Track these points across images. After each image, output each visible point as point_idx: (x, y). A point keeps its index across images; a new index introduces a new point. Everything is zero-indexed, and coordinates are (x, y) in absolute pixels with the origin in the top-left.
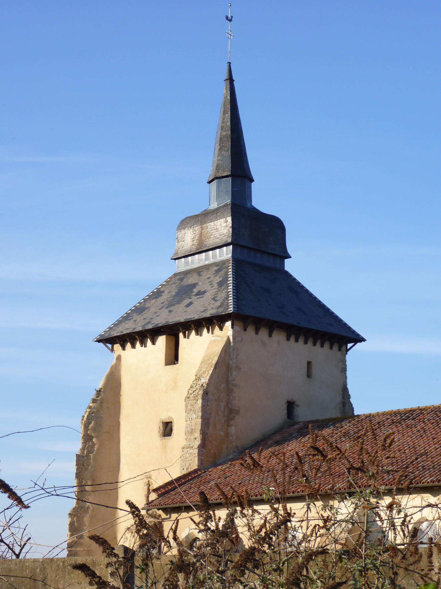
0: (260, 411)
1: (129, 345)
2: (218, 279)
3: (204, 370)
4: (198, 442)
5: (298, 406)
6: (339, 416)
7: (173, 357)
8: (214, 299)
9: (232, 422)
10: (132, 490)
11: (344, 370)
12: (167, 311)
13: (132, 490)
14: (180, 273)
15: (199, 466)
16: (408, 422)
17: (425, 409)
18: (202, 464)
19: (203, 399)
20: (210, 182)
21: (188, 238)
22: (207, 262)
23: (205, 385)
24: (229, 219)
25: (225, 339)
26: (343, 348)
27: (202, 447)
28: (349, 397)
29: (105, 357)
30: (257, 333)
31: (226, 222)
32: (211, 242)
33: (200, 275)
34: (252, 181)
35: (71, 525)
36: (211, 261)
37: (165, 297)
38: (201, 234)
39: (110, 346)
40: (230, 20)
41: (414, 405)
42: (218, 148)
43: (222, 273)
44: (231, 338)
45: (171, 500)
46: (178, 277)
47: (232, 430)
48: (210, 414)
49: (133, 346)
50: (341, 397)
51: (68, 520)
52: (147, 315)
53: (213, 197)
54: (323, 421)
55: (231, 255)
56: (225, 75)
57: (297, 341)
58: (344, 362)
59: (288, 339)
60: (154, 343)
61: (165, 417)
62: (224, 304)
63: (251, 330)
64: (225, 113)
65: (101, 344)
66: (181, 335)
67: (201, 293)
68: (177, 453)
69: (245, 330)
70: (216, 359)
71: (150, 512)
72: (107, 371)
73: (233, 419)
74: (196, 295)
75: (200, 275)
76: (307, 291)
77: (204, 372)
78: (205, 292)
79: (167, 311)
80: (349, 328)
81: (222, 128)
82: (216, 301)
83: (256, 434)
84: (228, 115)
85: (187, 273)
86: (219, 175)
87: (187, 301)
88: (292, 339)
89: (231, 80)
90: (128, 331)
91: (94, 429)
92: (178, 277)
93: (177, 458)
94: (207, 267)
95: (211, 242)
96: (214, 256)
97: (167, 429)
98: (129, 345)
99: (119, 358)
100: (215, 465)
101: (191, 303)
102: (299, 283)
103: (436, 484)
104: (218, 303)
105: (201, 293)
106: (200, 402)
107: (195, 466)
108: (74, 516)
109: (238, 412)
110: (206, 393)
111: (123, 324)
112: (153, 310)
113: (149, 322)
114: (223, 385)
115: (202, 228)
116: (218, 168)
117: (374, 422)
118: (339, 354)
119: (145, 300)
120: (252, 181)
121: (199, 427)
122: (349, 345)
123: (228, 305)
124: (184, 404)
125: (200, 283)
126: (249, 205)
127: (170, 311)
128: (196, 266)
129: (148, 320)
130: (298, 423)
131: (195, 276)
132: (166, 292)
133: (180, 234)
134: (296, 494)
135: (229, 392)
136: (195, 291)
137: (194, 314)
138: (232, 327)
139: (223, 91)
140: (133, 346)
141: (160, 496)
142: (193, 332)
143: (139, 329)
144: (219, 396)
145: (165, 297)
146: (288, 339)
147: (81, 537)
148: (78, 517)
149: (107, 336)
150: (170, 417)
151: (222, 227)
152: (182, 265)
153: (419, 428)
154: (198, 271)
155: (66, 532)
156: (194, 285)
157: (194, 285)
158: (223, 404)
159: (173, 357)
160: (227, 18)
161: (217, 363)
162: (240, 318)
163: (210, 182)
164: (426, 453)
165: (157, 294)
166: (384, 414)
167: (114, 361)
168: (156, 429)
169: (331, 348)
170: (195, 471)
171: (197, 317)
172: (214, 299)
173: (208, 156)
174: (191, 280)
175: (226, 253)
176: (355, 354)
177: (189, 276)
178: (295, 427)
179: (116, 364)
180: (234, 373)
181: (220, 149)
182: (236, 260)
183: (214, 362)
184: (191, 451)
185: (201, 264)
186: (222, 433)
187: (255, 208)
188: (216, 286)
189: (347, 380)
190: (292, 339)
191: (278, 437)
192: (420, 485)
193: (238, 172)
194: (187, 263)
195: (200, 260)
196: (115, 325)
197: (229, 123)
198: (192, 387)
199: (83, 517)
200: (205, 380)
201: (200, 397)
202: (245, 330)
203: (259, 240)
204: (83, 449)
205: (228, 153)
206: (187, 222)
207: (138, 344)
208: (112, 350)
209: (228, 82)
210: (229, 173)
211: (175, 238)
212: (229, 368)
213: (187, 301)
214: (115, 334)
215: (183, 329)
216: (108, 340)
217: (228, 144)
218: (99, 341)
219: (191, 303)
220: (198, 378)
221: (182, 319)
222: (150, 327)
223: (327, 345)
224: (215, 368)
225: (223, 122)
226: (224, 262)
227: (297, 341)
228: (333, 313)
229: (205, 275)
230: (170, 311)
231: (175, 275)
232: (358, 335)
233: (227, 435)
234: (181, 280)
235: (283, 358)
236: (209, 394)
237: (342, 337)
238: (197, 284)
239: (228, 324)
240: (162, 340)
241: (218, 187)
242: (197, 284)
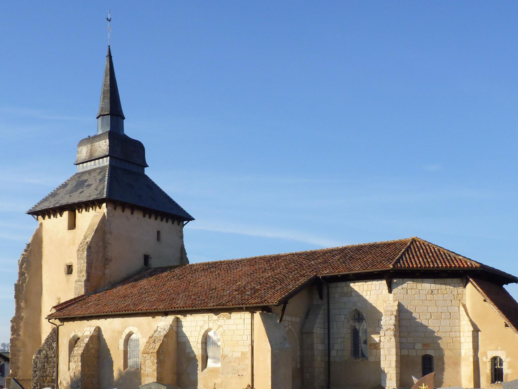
0: (125, 260)
1: (47, 217)
2: (100, 177)
3: (89, 233)
4: (85, 278)
5: (151, 258)
6: (178, 264)
7: (72, 225)
8: (96, 189)
9: (107, 266)
10: (47, 306)
11: (182, 237)
12: (68, 196)
13: (47, 306)
14: (79, 173)
15: (85, 293)
16: (212, 270)
17: (223, 262)
18: (87, 292)
19: (88, 251)
20: (98, 118)
21: (84, 152)
22: (95, 167)
23: (89, 242)
24: (107, 141)
25: (102, 214)
26: (181, 224)
27: (87, 281)
28: (186, 254)
29: (32, 224)
30: (123, 212)
31: (106, 142)
32: (97, 155)
33: (90, 175)
34: (124, 118)
35: (12, 327)
36: (97, 166)
37: (69, 187)
38: (91, 150)
39: (36, 217)
40: (110, 21)
41: (218, 260)
42: (102, 97)
43: (102, 174)
44: (106, 214)
45: (66, 313)
46: (78, 176)
47: (107, 271)
48: (93, 260)
49: (49, 217)
50: (180, 254)
51: (10, 324)
52: (57, 198)
53: (100, 127)
54: (164, 268)
55: (108, 163)
56: (107, 53)
57: (150, 218)
58: (181, 232)
59: (144, 216)
60: (61, 216)
61: (68, 262)
62: (101, 193)
63: (119, 210)
64: (106, 76)
65: (30, 215)
66: (77, 211)
67: (89, 186)
68: (73, 285)
69: (115, 209)
70: (96, 226)
71: (50, 321)
72: (34, 232)
73: (108, 264)
74: (86, 187)
75: (90, 175)
76: (159, 187)
77: (89, 234)
78: (91, 185)
79: (68, 196)
80: (185, 211)
81: (105, 85)
82: (97, 190)
83: (123, 274)
84: (108, 77)
85: (83, 173)
86: (103, 114)
87: (81, 190)
88: (147, 216)
89: (110, 56)
90: (45, 208)
91: (26, 268)
92: (78, 176)
93: (71, 288)
94: (94, 170)
95: (97, 154)
96: (99, 164)
97: (69, 269)
98: (47, 217)
99: (41, 225)
100: (95, 293)
101: (83, 191)
102: (153, 183)
103: (216, 307)
104: (98, 192)
105: (89, 186)
106: (85, 253)
107: (82, 293)
108: (14, 322)
109: (111, 260)
110: (89, 248)
111: (43, 204)
112: (61, 195)
113: (58, 203)
114: (101, 243)
115: (92, 146)
116: (102, 109)
117: (193, 269)
118: (178, 227)
119: (58, 189)
120: (124, 118)
121: (85, 269)
122: (185, 222)
123: (103, 193)
124: (76, 253)
125: (89, 180)
126: (122, 133)
127: (70, 196)
128: (89, 169)
129: (57, 201)
130: (150, 269)
131: (87, 175)
132: (70, 184)
133: (80, 149)
134: (135, 312)
135: (105, 247)
136: (86, 184)
137: (83, 198)
138: (107, 207)
139: (106, 63)
140: (49, 217)
141: (57, 311)
142: (84, 210)
143: (52, 206)
144: (98, 250)
145: (69, 187)
146: (144, 216)
147: (19, 335)
148: (16, 323)
149: (33, 210)
150: (71, 263)
151: (103, 146)
152: (81, 168)
153: (216, 273)
154: (89, 172)
155: (10, 332)
156: (86, 181)
157: (86, 181)
158: (101, 255)
159: (72, 225)
160: (107, 19)
161: (96, 229)
162: (111, 200)
163: (98, 118)
164: (215, 289)
165: (64, 186)
166: (200, 264)
167: (38, 227)
168: (63, 269)
169: (173, 223)
170: (82, 296)
171: (85, 200)
172: (96, 189)
173: (97, 102)
174: (84, 178)
175: (106, 162)
176: (188, 228)
177: (84, 175)
178: (149, 271)
179: (39, 228)
180: (108, 236)
181: (103, 98)
182: (112, 166)
183: (95, 228)
184: (80, 283)
185: (92, 168)
186: (101, 273)
187: (125, 135)
188: (98, 181)
189: (184, 243)
190: (147, 216)
191: (137, 277)
192: (206, 308)
193: (115, 112)
194: (83, 167)
195: (91, 166)
196: (39, 204)
197: (109, 82)
198: (81, 243)
199: (19, 323)
200: (89, 239)
201: (85, 250)
202: (115, 209)
203: (127, 156)
204: (19, 280)
205: (108, 101)
206: (83, 142)
207: (52, 216)
208: (37, 219)
209: (108, 57)
210: (109, 113)
211: (82, 153)
212: (104, 232)
213: (81, 190)
214: (38, 209)
215: (78, 207)
216: (37, 213)
217: (108, 95)
218: (29, 213)
219: (83, 191)
220: (85, 238)
221: (76, 201)
222: (58, 205)
223: (170, 222)
224: (96, 232)
225: (105, 82)
226: (104, 167)
227: (150, 218)
228: (174, 202)
229: (93, 175)
230: (70, 196)
231: (76, 174)
232: (190, 216)
233: (104, 274)
234: (79, 177)
235: (142, 229)
236: (92, 248)
237: (181, 217)
238: (87, 180)
239: (104, 205)
240: (66, 214)
241: (102, 121)
242: (87, 180)
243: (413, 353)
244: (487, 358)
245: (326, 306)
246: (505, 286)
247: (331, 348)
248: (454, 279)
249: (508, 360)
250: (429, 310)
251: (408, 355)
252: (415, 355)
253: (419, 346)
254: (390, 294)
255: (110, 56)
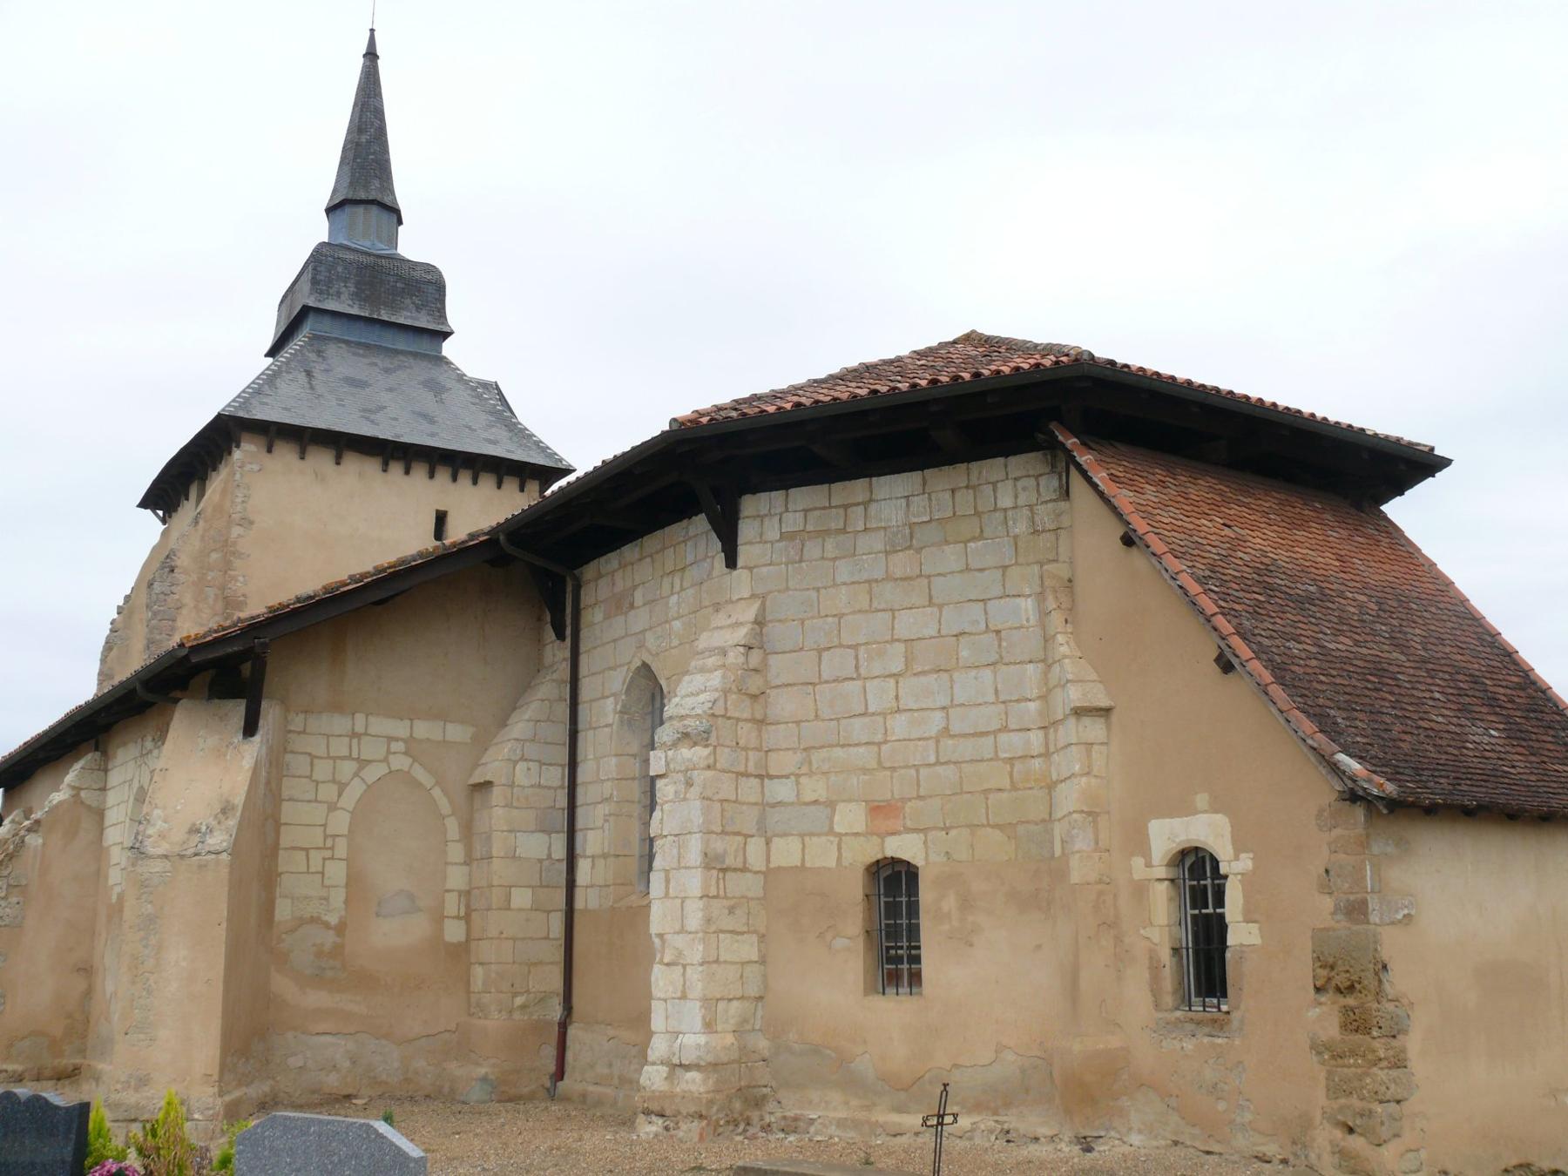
69: (269, 451)
89: (371, 55)
202: (269, 451)
243: (822, 855)
244: (1149, 865)
245: (564, 670)
246: (1383, 508)
247: (578, 850)
248: (1014, 461)
249: (1245, 863)
250: (902, 631)
251: (802, 868)
252: (831, 863)
253: (850, 817)
254: (735, 573)
255: (371, 55)
